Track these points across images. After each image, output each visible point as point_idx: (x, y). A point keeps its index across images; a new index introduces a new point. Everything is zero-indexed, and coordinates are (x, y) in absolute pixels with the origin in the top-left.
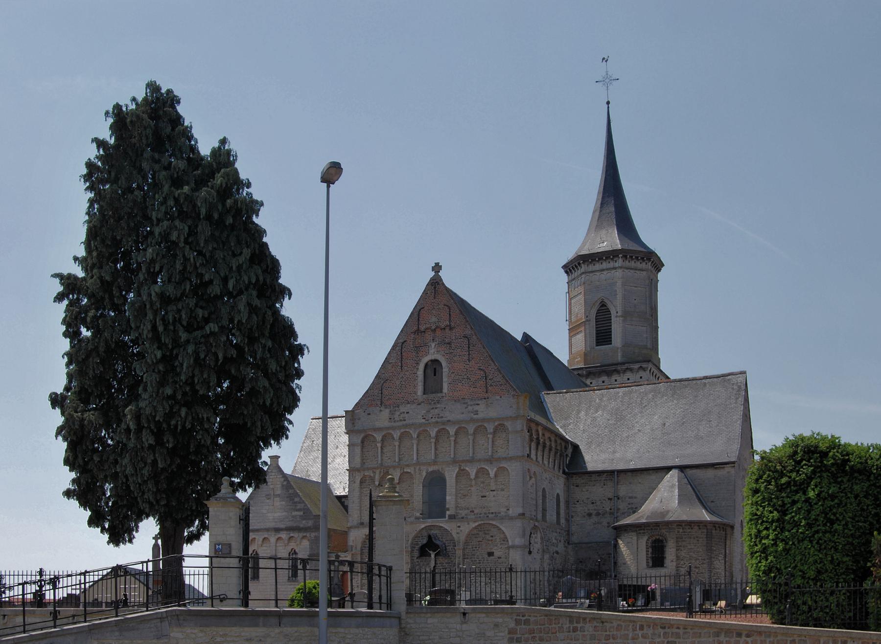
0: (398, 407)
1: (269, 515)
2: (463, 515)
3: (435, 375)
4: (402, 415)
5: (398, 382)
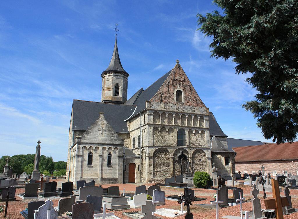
0: (168, 104)
1: (99, 137)
5: (167, 95)
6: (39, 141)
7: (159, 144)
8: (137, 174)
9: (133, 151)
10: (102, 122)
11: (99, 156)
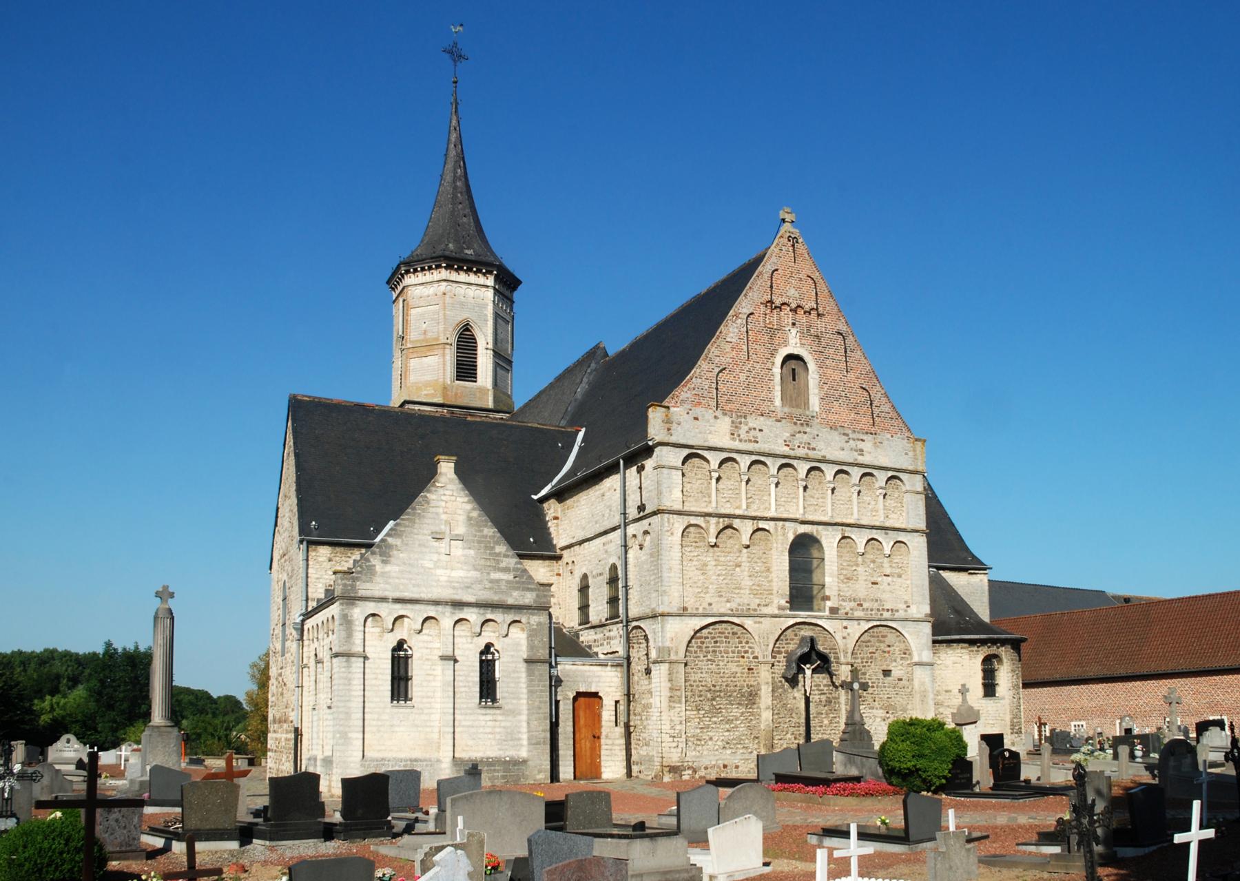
0: (745, 417)
1: (439, 572)
2: (848, 609)
3: (794, 379)
4: (752, 433)
5: (743, 377)
6: (166, 588)
7: (710, 604)
8: (610, 742)
9: (581, 639)
10: (448, 500)
11: (443, 658)
